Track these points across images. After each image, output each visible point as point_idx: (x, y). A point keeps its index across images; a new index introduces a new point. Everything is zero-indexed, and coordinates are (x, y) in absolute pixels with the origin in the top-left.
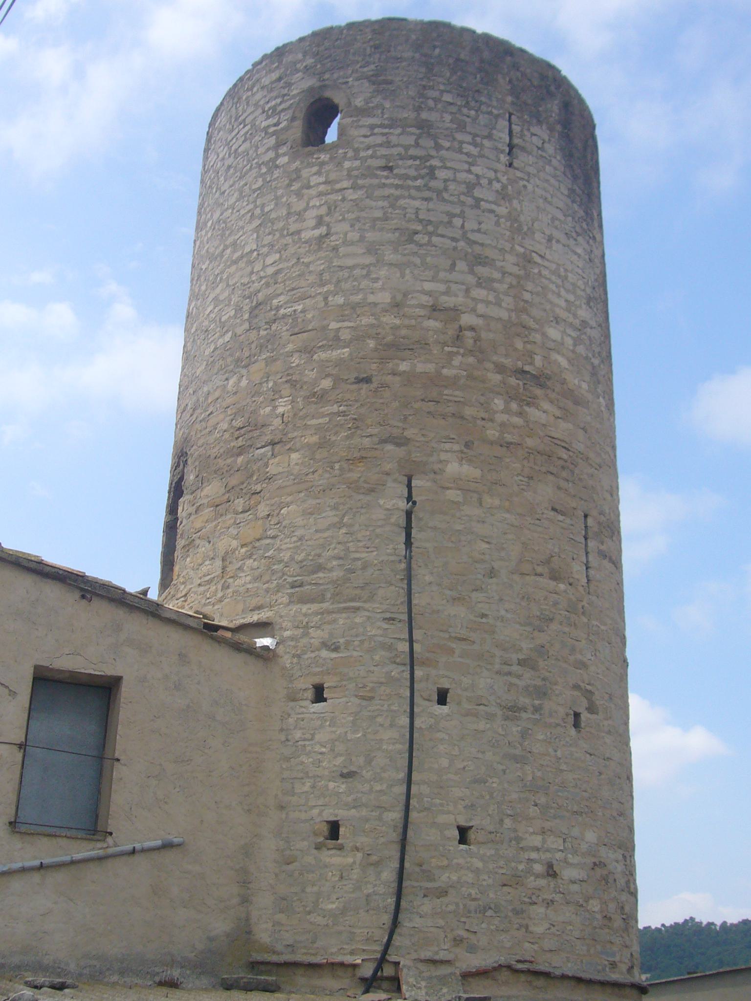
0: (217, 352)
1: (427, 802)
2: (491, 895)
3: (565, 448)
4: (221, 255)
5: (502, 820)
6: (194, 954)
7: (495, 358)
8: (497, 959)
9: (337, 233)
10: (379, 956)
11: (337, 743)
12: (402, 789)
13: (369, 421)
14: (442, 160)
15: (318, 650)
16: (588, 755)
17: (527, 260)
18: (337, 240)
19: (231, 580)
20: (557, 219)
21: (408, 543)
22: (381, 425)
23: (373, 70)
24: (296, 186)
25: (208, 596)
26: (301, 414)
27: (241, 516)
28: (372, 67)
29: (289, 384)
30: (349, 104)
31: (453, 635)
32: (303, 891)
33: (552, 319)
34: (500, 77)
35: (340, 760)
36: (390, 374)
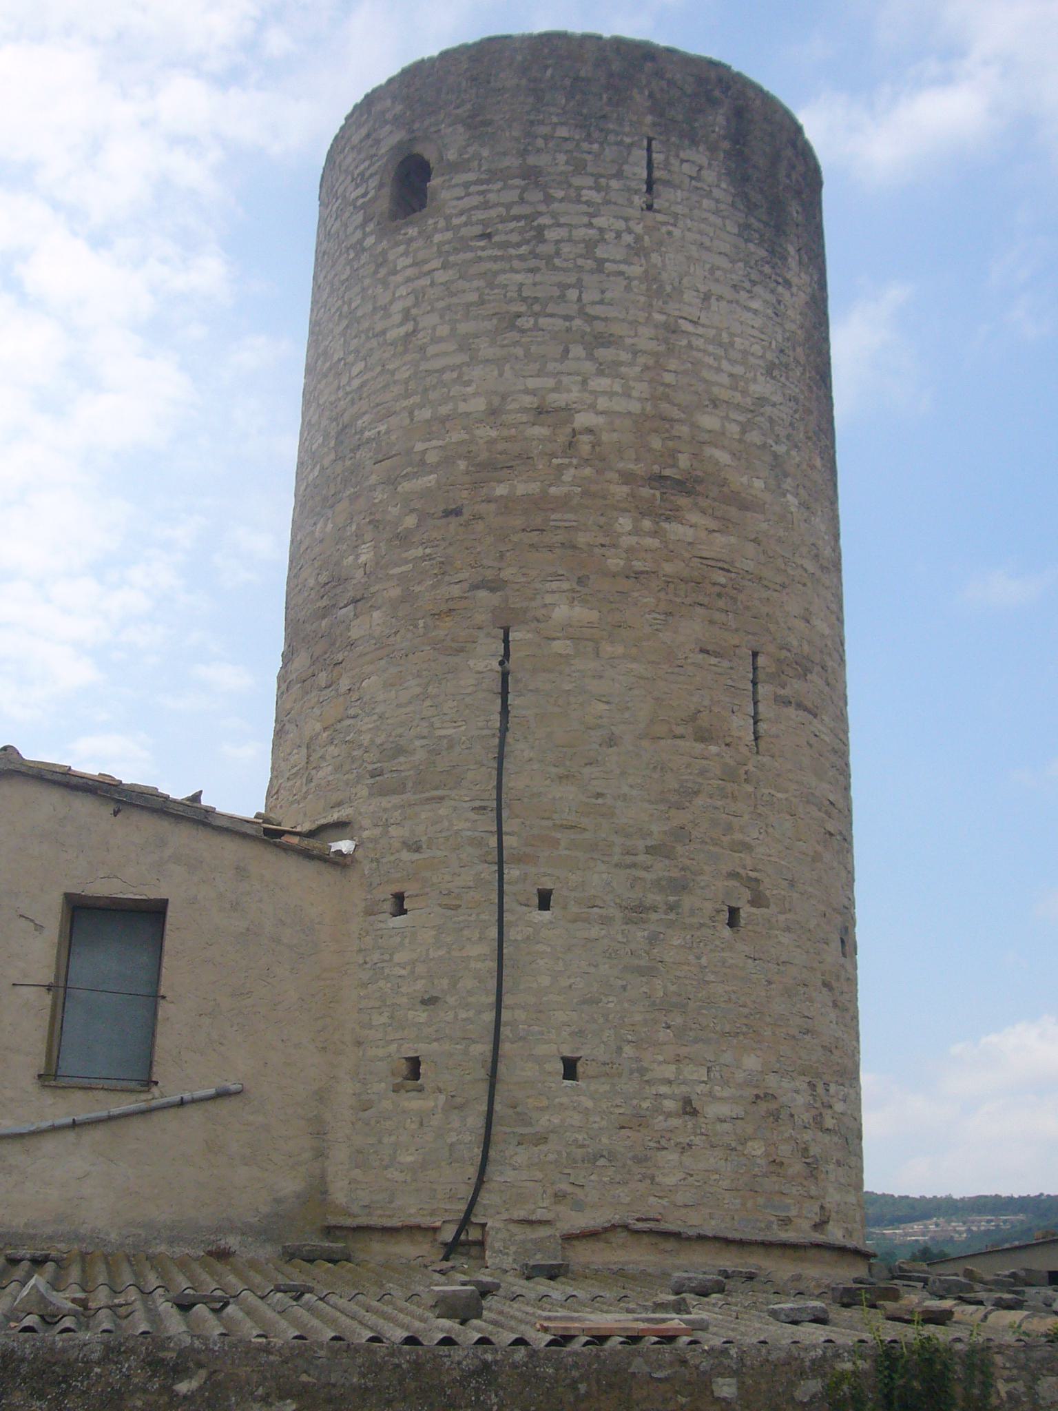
0: (309, 489)
1: (523, 1029)
2: (605, 1140)
3: (723, 569)
6: (257, 1219)
7: (621, 465)
8: (610, 1218)
9: (424, 328)
12: (490, 1016)
13: (458, 563)
14: (554, 215)
16: (750, 961)
19: (313, 772)
20: (718, 268)
21: (505, 711)
24: (383, 272)
25: (295, 792)
29: (372, 526)
30: (441, 159)
31: (557, 822)
32: (380, 1142)
33: (707, 403)
35: (420, 984)
36: (483, 501)
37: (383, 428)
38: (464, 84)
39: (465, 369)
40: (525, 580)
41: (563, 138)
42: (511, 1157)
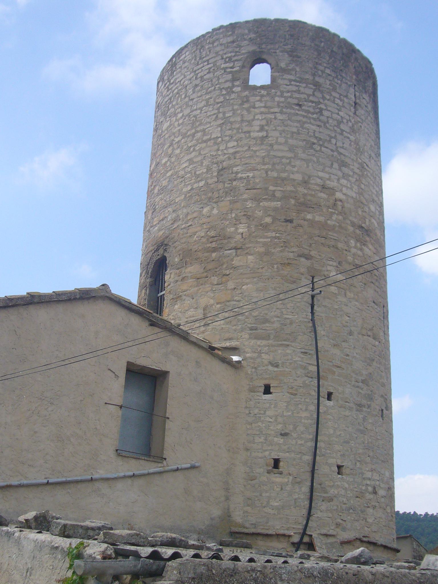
2: (352, 502)
4: (193, 135)
5: (356, 463)
6: (204, 527)
9: (272, 137)
10: (301, 531)
11: (279, 417)
12: (312, 444)
13: (292, 244)
14: (326, 105)
15: (267, 365)
17: (362, 167)
18: (272, 141)
21: (312, 313)
22: (298, 247)
23: (290, 48)
24: (246, 106)
26: (254, 234)
27: (216, 286)
28: (289, 46)
31: (335, 364)
32: (261, 495)
34: (350, 64)
35: (280, 427)
36: (302, 219)
37: (251, 175)
38: (287, 36)
39: (292, 160)
40: (319, 257)
41: (328, 74)
42: (320, 506)
